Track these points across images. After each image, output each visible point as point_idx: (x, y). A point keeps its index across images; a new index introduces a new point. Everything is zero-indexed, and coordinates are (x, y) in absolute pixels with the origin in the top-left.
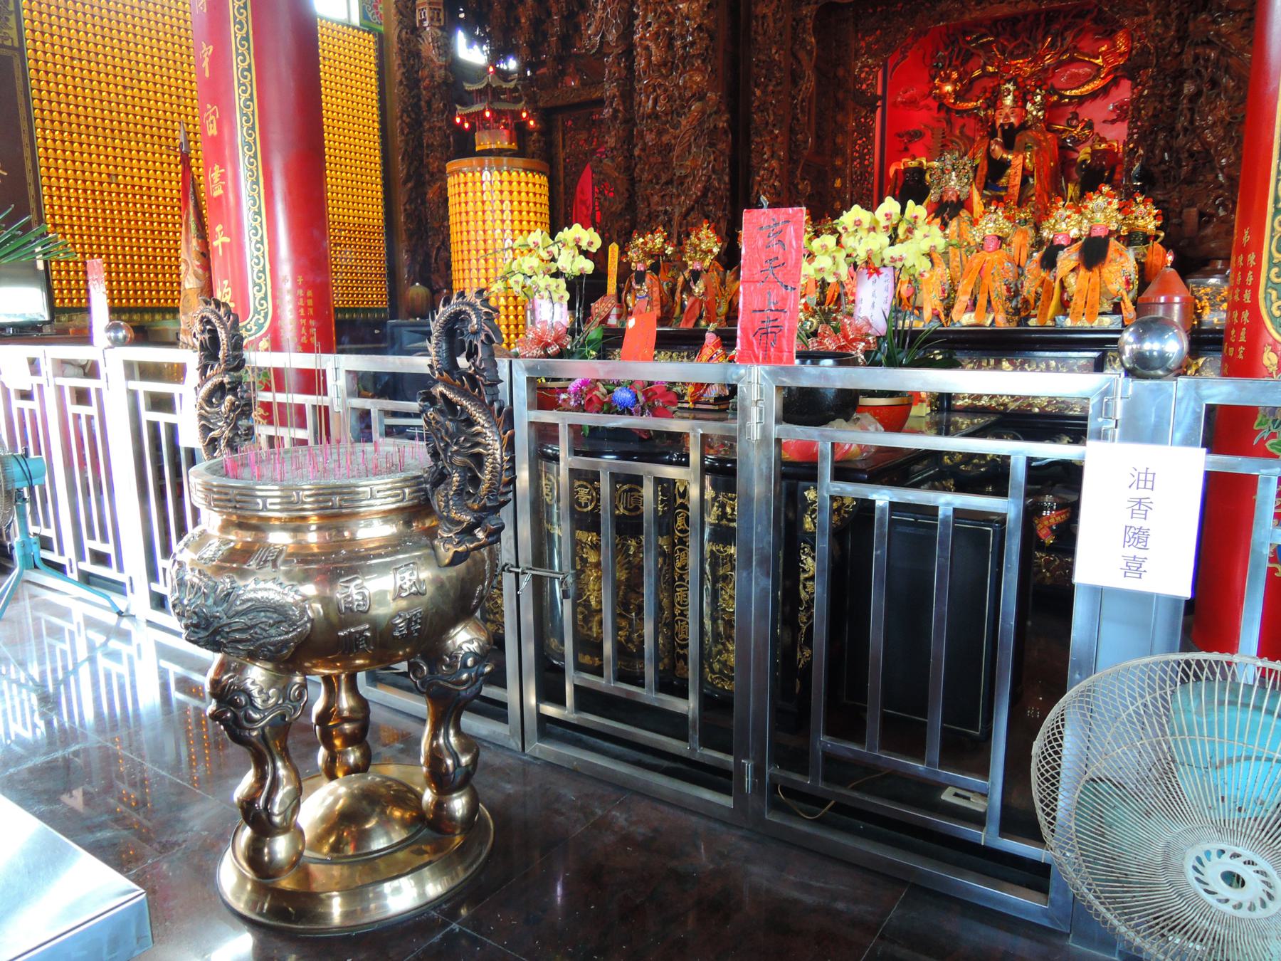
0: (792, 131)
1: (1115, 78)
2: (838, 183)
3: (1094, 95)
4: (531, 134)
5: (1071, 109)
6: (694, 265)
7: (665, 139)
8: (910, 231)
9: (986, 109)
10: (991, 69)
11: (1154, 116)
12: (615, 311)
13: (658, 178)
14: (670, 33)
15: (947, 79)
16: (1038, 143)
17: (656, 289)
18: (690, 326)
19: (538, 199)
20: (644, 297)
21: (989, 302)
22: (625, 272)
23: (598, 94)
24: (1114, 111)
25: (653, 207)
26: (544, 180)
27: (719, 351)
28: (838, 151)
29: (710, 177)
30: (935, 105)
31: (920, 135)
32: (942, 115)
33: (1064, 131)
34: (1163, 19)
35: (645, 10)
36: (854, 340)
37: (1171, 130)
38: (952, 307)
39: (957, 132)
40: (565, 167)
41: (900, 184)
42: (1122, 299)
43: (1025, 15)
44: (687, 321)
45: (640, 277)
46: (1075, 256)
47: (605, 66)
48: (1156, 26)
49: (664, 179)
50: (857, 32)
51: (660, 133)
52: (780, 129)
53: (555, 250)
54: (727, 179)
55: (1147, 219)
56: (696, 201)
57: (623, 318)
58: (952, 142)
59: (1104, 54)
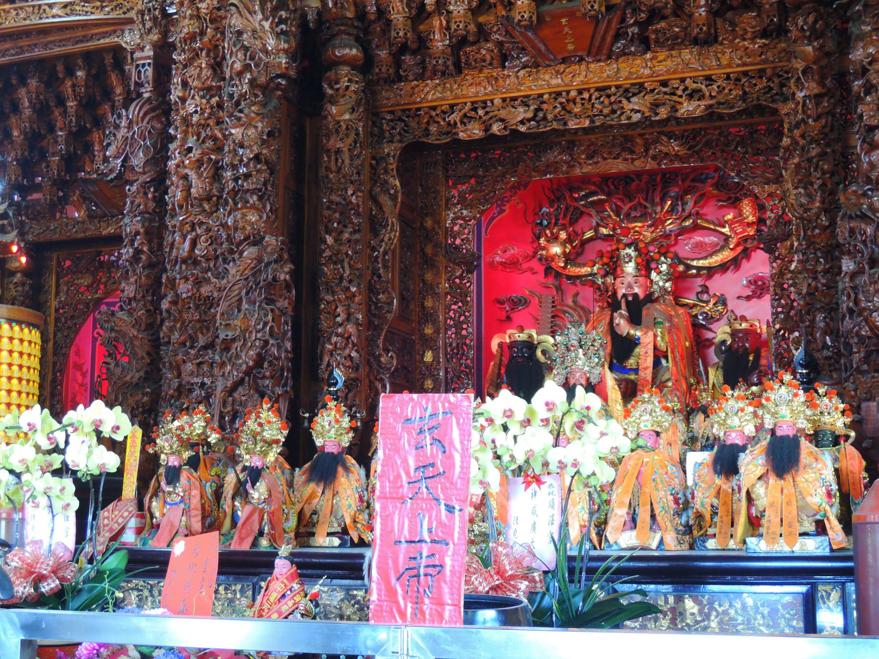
0: (371, 290)
1: (745, 250)
2: (429, 357)
3: (723, 268)
4: (13, 274)
5: (699, 281)
6: (250, 461)
7: (205, 290)
8: (579, 425)
9: (604, 276)
10: (604, 231)
11: (809, 294)
12: (133, 523)
13: (193, 339)
14: (217, 162)
15: (555, 238)
16: (670, 318)
17: (196, 493)
18: (246, 547)
19: (25, 361)
20: (175, 505)
21: (653, 517)
22: (149, 466)
23: (111, 230)
24: (747, 286)
25: (186, 378)
26: (35, 336)
27: (296, 586)
28: (428, 317)
29: (266, 342)
30: (541, 269)
31: (526, 303)
32: (550, 282)
33: (695, 306)
34: (805, 188)
35: (186, 133)
36: (512, 577)
37: (832, 309)
38: (605, 522)
39: (570, 302)
40: (57, 320)
41: (505, 360)
42: (825, 515)
43: (639, 174)
44: (241, 540)
45: (173, 475)
46: (761, 460)
47: (126, 196)
48: (795, 194)
49: (202, 341)
50: (447, 178)
51: (198, 283)
52: (359, 285)
53: (60, 437)
54: (288, 345)
55: (835, 417)
56: (248, 373)
57: (145, 534)
58: (565, 312)
59: (731, 223)
